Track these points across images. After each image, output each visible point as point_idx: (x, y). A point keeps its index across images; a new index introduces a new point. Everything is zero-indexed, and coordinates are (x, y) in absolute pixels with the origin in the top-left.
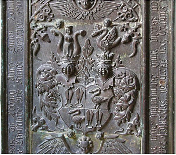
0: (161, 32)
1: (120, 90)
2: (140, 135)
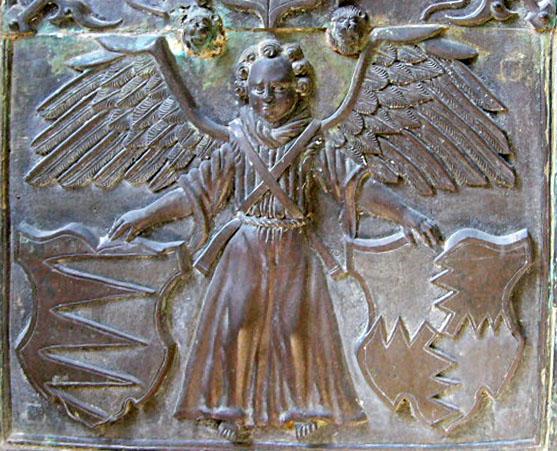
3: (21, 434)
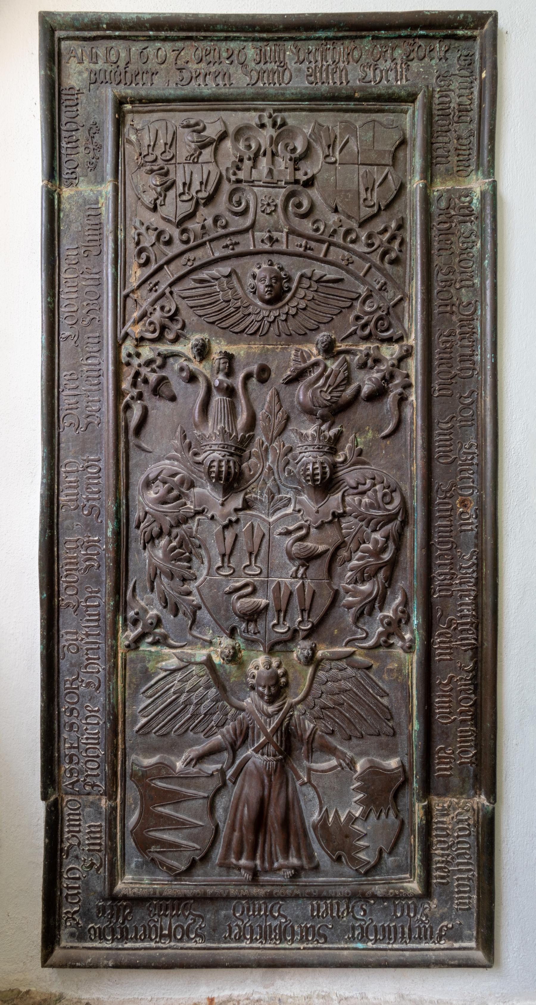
0: (461, 370)
1: (361, 523)
2: (410, 647)
3: (131, 877)
